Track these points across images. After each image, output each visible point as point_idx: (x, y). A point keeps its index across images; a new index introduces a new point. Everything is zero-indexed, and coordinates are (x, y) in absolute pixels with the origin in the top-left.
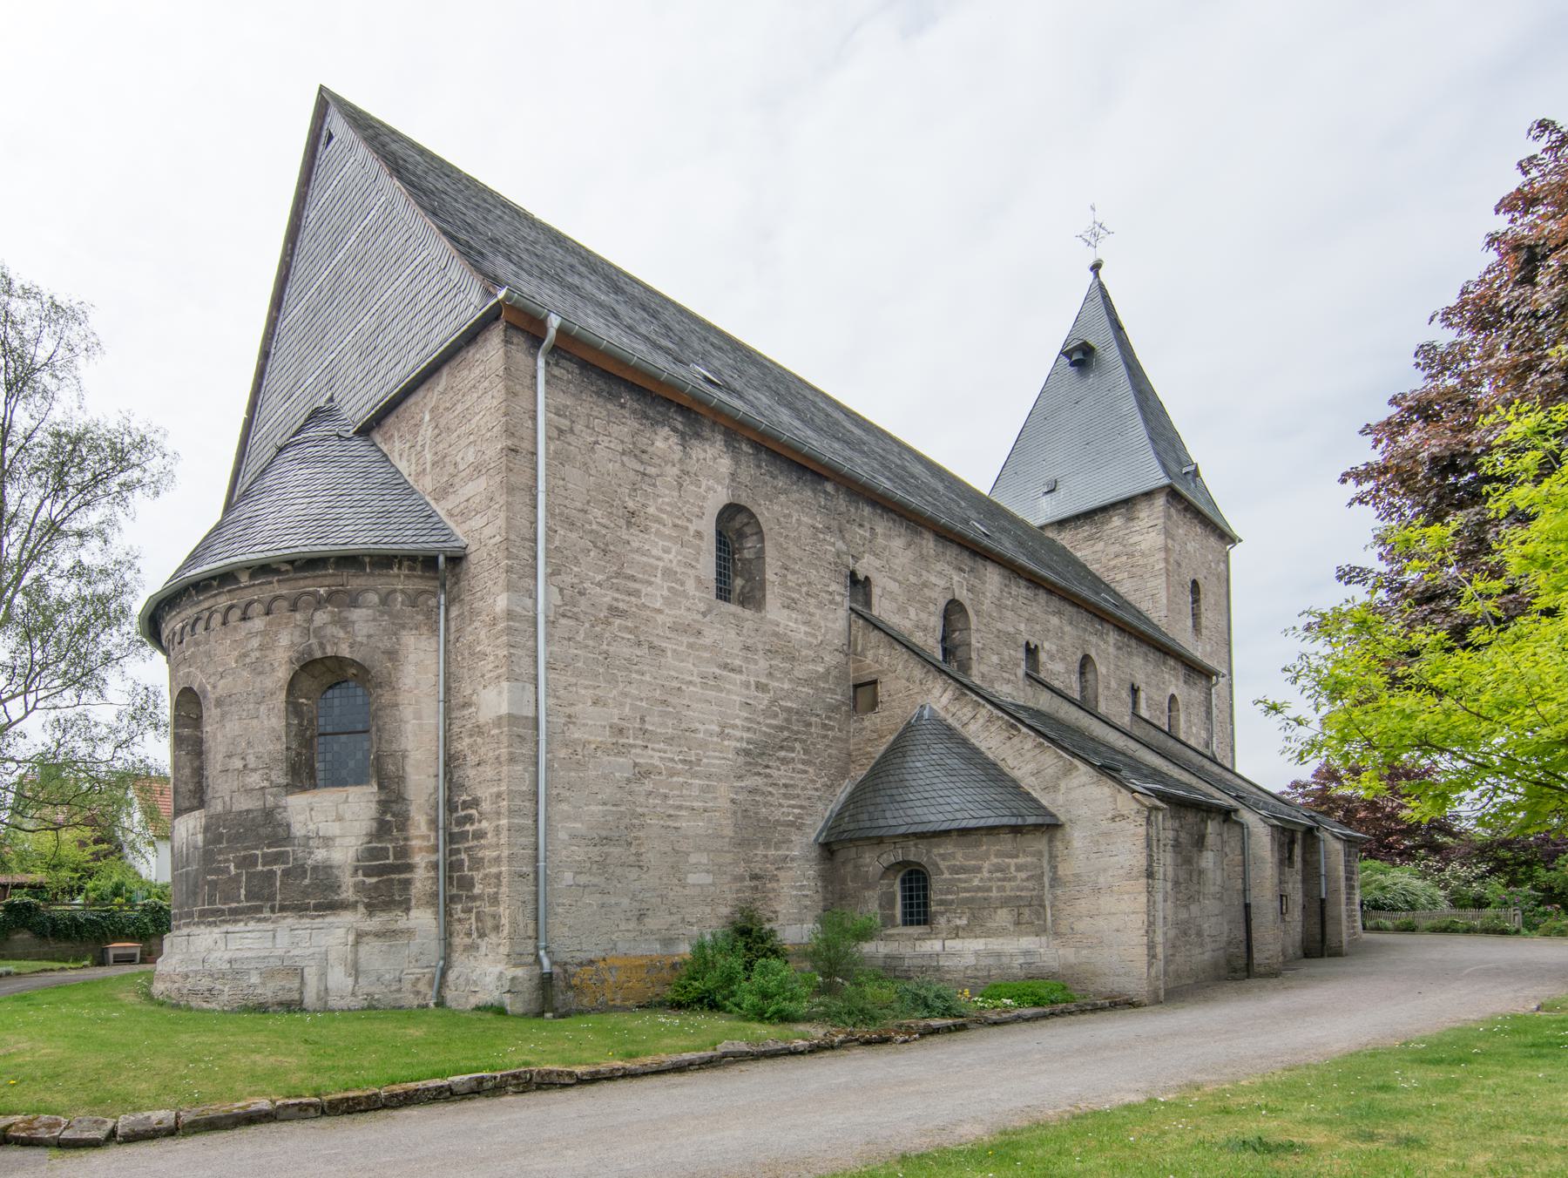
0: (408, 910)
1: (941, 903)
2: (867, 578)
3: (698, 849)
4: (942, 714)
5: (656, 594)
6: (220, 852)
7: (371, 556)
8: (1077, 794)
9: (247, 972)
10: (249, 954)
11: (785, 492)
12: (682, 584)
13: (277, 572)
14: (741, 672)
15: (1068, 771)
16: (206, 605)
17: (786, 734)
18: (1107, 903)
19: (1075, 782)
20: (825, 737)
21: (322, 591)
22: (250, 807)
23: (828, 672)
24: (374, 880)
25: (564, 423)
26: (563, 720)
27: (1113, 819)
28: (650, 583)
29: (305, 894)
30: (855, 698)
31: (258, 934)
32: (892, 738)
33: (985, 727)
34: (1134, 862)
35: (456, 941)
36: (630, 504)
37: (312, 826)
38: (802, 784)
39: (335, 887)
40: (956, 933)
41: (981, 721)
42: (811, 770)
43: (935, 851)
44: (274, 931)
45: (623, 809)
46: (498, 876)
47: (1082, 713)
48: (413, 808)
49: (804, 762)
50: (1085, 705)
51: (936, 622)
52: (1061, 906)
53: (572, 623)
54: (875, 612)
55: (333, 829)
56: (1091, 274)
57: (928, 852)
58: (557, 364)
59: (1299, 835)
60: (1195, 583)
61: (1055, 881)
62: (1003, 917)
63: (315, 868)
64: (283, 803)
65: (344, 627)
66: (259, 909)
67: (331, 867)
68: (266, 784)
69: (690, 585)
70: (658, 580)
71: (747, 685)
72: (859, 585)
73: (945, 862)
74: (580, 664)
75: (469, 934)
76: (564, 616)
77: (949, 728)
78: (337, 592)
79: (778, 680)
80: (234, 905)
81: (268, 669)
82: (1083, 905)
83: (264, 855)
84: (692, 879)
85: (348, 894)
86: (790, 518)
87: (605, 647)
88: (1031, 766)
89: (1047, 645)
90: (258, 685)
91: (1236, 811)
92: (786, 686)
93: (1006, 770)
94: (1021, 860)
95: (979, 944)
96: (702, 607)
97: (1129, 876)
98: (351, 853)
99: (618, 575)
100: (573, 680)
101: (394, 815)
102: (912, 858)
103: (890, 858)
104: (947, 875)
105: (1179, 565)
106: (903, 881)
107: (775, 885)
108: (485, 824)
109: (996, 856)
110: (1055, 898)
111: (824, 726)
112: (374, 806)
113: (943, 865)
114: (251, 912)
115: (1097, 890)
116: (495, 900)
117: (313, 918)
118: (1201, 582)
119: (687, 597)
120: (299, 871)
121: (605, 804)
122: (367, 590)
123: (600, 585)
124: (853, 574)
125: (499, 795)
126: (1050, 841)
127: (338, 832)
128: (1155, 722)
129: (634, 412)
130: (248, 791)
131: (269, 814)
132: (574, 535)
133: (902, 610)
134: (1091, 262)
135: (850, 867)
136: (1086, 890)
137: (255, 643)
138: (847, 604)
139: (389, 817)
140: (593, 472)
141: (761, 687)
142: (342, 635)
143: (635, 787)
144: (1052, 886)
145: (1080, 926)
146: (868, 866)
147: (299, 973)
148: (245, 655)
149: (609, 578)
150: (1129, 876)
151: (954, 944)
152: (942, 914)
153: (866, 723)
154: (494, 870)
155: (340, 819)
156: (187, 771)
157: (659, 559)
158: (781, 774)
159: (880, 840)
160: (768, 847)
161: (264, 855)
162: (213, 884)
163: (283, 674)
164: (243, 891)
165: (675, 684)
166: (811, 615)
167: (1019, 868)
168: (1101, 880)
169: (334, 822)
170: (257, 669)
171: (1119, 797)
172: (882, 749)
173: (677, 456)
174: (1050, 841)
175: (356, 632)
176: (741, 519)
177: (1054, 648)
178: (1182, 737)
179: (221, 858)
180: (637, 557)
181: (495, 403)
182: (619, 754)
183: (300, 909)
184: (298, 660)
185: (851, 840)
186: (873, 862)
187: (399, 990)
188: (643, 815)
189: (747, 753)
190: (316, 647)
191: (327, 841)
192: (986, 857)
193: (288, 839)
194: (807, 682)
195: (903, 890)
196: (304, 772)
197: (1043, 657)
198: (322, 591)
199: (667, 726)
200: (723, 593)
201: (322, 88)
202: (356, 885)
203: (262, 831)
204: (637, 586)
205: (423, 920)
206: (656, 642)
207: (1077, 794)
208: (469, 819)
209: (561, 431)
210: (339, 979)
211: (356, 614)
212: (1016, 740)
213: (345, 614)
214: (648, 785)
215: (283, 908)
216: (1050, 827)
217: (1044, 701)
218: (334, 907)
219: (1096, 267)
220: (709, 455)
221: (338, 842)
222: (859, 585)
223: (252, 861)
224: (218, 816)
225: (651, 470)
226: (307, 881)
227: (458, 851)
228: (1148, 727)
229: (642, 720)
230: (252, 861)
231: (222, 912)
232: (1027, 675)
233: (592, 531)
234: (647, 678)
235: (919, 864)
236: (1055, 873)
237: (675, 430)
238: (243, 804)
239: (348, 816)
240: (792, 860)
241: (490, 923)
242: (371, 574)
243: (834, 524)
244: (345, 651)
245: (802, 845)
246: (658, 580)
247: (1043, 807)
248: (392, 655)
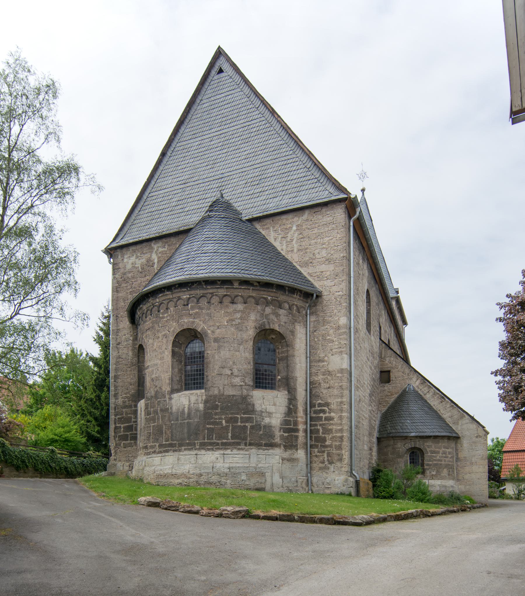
0: (297, 450)
1: (428, 465)
4: (416, 389)
6: (216, 414)
7: (289, 287)
8: (465, 426)
9: (240, 473)
10: (238, 465)
13: (252, 285)
16: (211, 291)
18: (475, 468)
19: (464, 422)
21: (269, 298)
22: (235, 394)
24: (286, 435)
27: (477, 437)
29: (261, 439)
31: (242, 456)
32: (396, 396)
33: (433, 397)
34: (484, 454)
35: (314, 465)
37: (263, 407)
39: (272, 436)
40: (432, 477)
41: (431, 394)
43: (426, 444)
44: (250, 455)
46: (341, 438)
48: (299, 403)
52: (460, 469)
55: (271, 409)
56: (361, 193)
57: (423, 444)
61: (458, 459)
62: (445, 472)
63: (265, 426)
64: (251, 394)
65: (276, 317)
66: (239, 444)
67: (271, 427)
68: (242, 384)
73: (429, 447)
75: (323, 462)
77: (421, 395)
78: (275, 300)
80: (225, 441)
81: (244, 329)
82: (467, 469)
83: (241, 418)
85: (277, 440)
88: (449, 414)
90: (239, 336)
93: (440, 414)
97: (482, 459)
98: (279, 421)
101: (293, 406)
102: (417, 446)
103: (409, 446)
104: (429, 454)
106: (410, 456)
108: (333, 414)
110: (458, 466)
112: (286, 400)
113: (428, 450)
114: (234, 445)
115: (472, 464)
116: (340, 448)
117: (264, 450)
120: (257, 427)
122: (285, 302)
125: (341, 402)
126: (456, 443)
127: (274, 411)
130: (234, 386)
131: (244, 398)
134: (361, 188)
135: (390, 449)
136: (468, 463)
137: (238, 315)
139: (291, 407)
142: (276, 320)
144: (456, 461)
145: (467, 477)
146: (400, 448)
147: (263, 474)
148: (233, 320)
150: (482, 459)
151: (432, 482)
152: (428, 469)
153: (386, 388)
154: (339, 435)
155: (275, 405)
156: (176, 370)
159: (406, 438)
161: (241, 418)
162: (211, 431)
163: (251, 333)
164: (230, 435)
167: (449, 453)
168: (473, 460)
169: (270, 405)
170: (239, 328)
171: (479, 429)
172: (393, 400)
174: (456, 443)
175: (279, 321)
179: (217, 417)
181: (339, 236)
183: (259, 445)
184: (259, 328)
185: (392, 437)
186: (402, 447)
187: (297, 486)
190: (266, 323)
191: (270, 414)
192: (440, 448)
193: (253, 411)
195: (410, 459)
196: (262, 379)
198: (269, 298)
201: (219, 47)
202: (280, 436)
203: (240, 406)
205: (301, 454)
207: (465, 426)
208: (324, 412)
210: (277, 479)
211: (281, 312)
212: (443, 403)
213: (277, 311)
215: (250, 444)
216: (456, 438)
218: (272, 445)
221: (274, 415)
223: (236, 420)
224: (215, 396)
226: (261, 432)
227: (316, 425)
230: (236, 420)
231: (218, 444)
236: (457, 456)
238: (230, 392)
239: (278, 404)
241: (336, 458)
242: (288, 295)
244: (277, 328)
247: (454, 430)
248: (293, 332)
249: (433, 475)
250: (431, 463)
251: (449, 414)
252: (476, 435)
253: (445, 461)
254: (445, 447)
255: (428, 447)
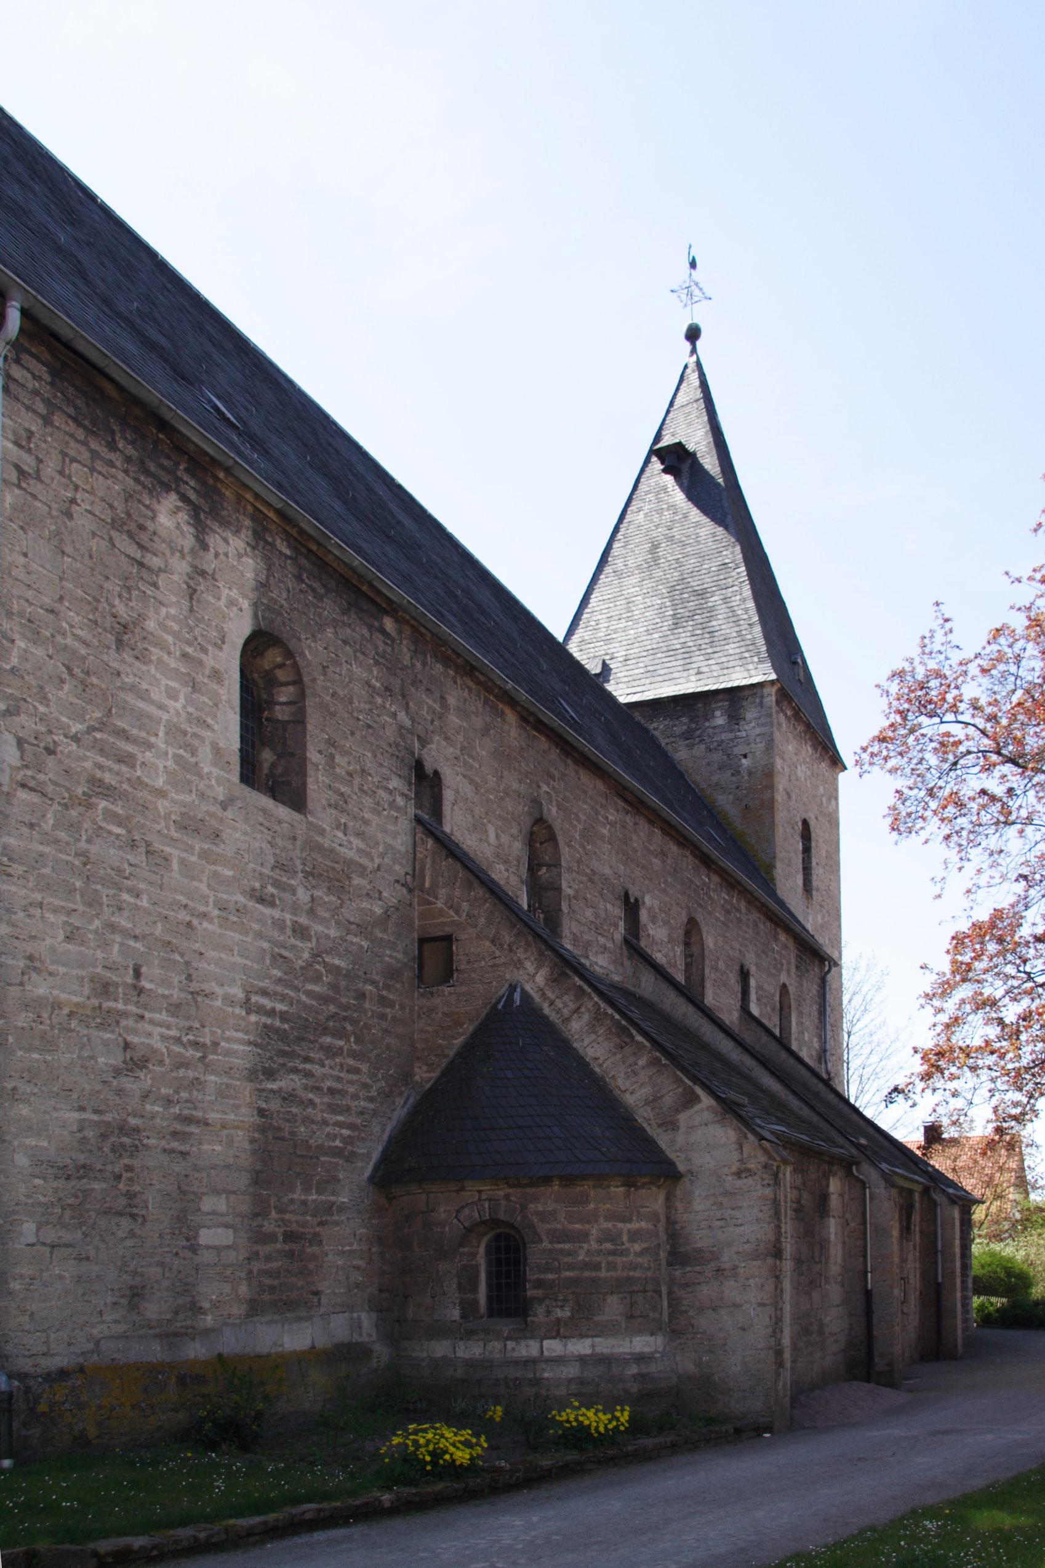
1: (539, 1284)
2: (436, 773)
3: (216, 1192)
4: (537, 997)
5: (158, 764)
11: (335, 624)
12: (194, 754)
14: (272, 904)
15: (689, 1100)
17: (332, 1008)
18: (730, 1290)
20: (382, 1017)
23: (386, 916)
25: (28, 462)
26: (21, 964)
27: (738, 1174)
28: (150, 746)
30: (421, 958)
33: (592, 1028)
36: (121, 609)
38: (352, 1089)
40: (557, 1331)
41: (586, 1017)
42: (365, 1067)
45: (108, 1117)
47: (681, 1001)
49: (353, 1054)
50: (691, 993)
51: (517, 848)
53: (35, 798)
54: (447, 829)
56: (687, 346)
58: (18, 361)
59: (917, 1196)
60: (805, 823)
69: (205, 753)
70: (160, 741)
71: (279, 925)
72: (426, 784)
74: (47, 871)
76: (23, 786)
79: (323, 920)
82: (706, 1292)
84: (206, 1237)
86: (340, 665)
87: (83, 845)
89: (647, 899)
91: (858, 1164)
92: (333, 933)
94: (634, 1226)
95: (580, 1347)
96: (220, 792)
99: (102, 726)
100: (38, 896)
104: (546, 1244)
105: (789, 797)
107: (315, 1249)
109: (608, 1218)
111: (383, 1001)
113: (542, 1228)
118: (812, 823)
119: (200, 775)
121: (82, 1109)
123: (76, 738)
124: (419, 766)
128: (765, 1021)
129: (128, 459)
132: (39, 652)
133: (478, 827)
138: (411, 811)
140: (69, 549)
141: (301, 932)
143: (127, 1083)
149: (91, 729)
150: (755, 1256)
151: (553, 1347)
152: (540, 1300)
157: (161, 707)
158: (325, 1072)
160: (307, 1190)
165: (183, 916)
166: (367, 822)
167: (634, 1236)
172: (458, 1042)
173: (188, 542)
176: (273, 656)
177: (656, 903)
178: (794, 1047)
180: (130, 698)
182: (101, 1026)
188: (137, 1130)
189: (282, 1035)
194: (362, 929)
197: (644, 916)
199: (170, 986)
200: (249, 774)
204: (130, 748)
206: (157, 846)
209: (21, 472)
212: (628, 1050)
214: (146, 1080)
217: (648, 985)
219: (693, 334)
220: (231, 551)
222: (426, 784)
225: (155, 562)
228: (759, 1030)
229: (137, 974)
232: (626, 941)
233: (65, 648)
234: (144, 902)
235: (511, 1226)
237: (184, 498)
240: (341, 1209)
243: (396, 683)
245: (351, 1185)
246: (160, 741)
249: (558, 1320)
250: (550, 1276)
251: (645, 1091)
252: (734, 1169)
253: (612, 1267)
254: (612, 1217)
255: (543, 1216)
